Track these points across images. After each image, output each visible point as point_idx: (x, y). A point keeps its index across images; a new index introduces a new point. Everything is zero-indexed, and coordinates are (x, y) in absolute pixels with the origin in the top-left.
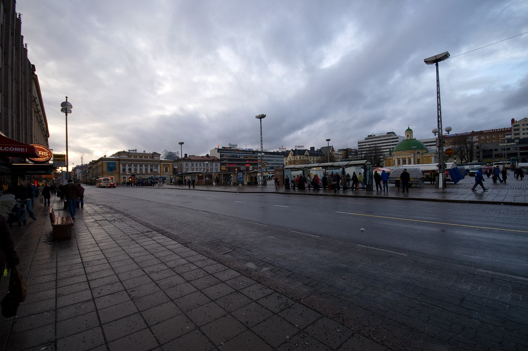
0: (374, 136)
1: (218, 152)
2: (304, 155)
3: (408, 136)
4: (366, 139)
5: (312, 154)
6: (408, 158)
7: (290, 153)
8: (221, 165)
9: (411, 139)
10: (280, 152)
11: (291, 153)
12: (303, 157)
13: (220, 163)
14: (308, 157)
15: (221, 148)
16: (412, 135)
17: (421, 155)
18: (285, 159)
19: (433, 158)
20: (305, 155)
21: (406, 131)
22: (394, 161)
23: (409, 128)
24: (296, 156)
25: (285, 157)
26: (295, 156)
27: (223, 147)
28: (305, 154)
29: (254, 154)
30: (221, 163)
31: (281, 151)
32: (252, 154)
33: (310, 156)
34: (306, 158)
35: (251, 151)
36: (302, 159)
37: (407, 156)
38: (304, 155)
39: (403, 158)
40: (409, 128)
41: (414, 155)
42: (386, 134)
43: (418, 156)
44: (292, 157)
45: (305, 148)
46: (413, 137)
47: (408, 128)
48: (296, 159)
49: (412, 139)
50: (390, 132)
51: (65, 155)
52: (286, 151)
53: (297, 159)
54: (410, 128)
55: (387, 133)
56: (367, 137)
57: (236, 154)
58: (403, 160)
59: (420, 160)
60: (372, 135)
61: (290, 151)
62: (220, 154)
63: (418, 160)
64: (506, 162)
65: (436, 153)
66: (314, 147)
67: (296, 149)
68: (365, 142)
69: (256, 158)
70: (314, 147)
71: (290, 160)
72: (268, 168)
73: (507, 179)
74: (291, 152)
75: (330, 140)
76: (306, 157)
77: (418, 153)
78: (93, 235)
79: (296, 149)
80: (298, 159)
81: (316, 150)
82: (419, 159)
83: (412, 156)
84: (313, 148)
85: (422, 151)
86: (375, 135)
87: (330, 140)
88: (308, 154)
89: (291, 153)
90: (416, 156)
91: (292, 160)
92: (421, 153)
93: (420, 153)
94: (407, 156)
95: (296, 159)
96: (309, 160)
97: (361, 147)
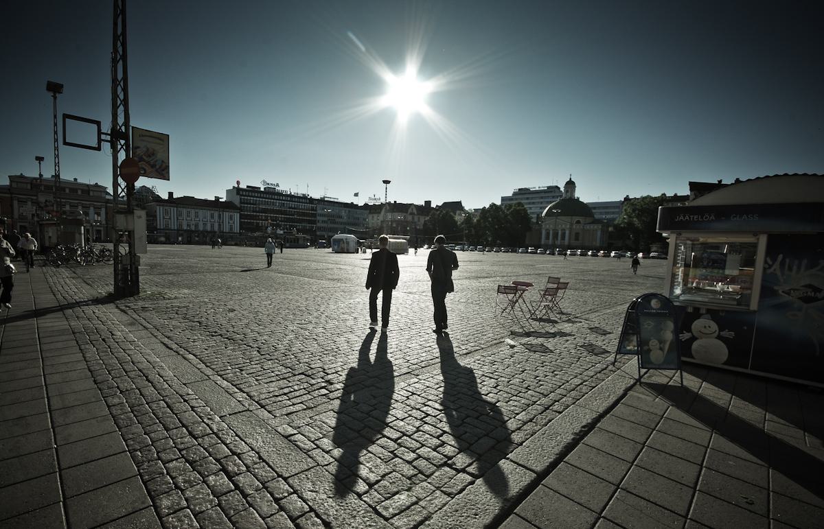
1: (238, 194)
2: (407, 213)
6: (547, 230)
8: (240, 218)
13: (238, 214)
15: (245, 187)
20: (409, 212)
25: (370, 213)
27: (248, 187)
28: (410, 211)
30: (240, 215)
33: (418, 214)
38: (407, 213)
41: (572, 224)
51: (162, 172)
57: (246, 198)
62: (241, 199)
66: (430, 202)
73: (451, 289)
77: (578, 222)
78: (114, 412)
81: (433, 205)
84: (428, 203)
88: (415, 211)
97: (607, 211)
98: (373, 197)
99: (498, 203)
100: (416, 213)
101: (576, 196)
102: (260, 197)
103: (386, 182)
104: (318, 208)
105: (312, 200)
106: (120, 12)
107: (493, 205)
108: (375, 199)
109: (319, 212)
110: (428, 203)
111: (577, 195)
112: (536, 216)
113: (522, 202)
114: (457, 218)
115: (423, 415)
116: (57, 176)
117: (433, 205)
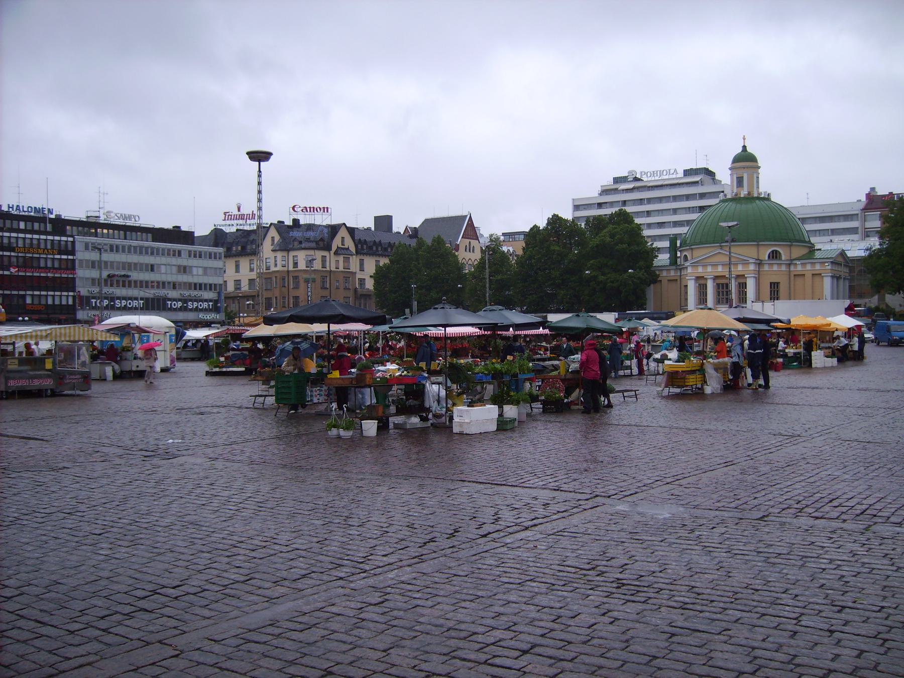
0: (636, 179)
3: (740, 181)
4: (605, 192)
5: (370, 248)
6: (698, 278)
7: (268, 240)
9: (750, 198)
10: (227, 230)
11: (273, 238)
12: (324, 257)
14: (346, 260)
16: (758, 178)
17: (784, 268)
18: (230, 265)
19: (827, 282)
20: (334, 248)
21: (737, 159)
22: (686, 286)
23: (744, 147)
24: (292, 254)
26: (288, 251)
28: (336, 243)
29: (63, 233)
31: (233, 229)
32: (46, 233)
33: (358, 252)
34: (337, 261)
35: (43, 220)
36: (317, 265)
37: (709, 269)
38: (328, 248)
39: (716, 278)
40: (744, 147)
41: (760, 263)
42: (681, 174)
43: (775, 272)
44: (272, 255)
45: (335, 221)
46: (758, 187)
47: (740, 150)
48: (291, 268)
49: (756, 195)
50: (694, 167)
52: (255, 227)
53: (296, 264)
54: (749, 150)
55: (687, 173)
56: (608, 181)
58: (718, 285)
59: (783, 289)
60: (626, 177)
61: (268, 228)
63: (774, 287)
64: (602, 335)
65: (840, 259)
66: (391, 217)
67: (296, 221)
68: (600, 205)
69: (67, 253)
70: (391, 217)
71: (268, 268)
72: (205, 305)
74: (273, 232)
75: (270, 154)
76: (341, 259)
77: (775, 255)
79: (296, 221)
80: (302, 266)
81: (398, 227)
82: (778, 283)
83: (752, 267)
84: (384, 222)
85: (788, 249)
86: (638, 176)
87: (270, 154)
88: (350, 244)
89: (273, 238)
90: (766, 268)
91: (273, 269)
92: (783, 258)
93: (780, 259)
94: (709, 269)
95: (291, 268)
96: (354, 274)
98: (236, 212)
99: (567, 214)
100: (353, 249)
101: (762, 190)
102: (33, 232)
103: (260, 157)
104: (78, 246)
105: (60, 225)
106: (2, 632)
107: (555, 220)
108: (242, 217)
109: (81, 255)
110: (384, 222)
111: (764, 187)
112: (666, 244)
113: (629, 209)
114: (463, 256)
115: (881, 641)
116: (501, 407)
117: (398, 227)
